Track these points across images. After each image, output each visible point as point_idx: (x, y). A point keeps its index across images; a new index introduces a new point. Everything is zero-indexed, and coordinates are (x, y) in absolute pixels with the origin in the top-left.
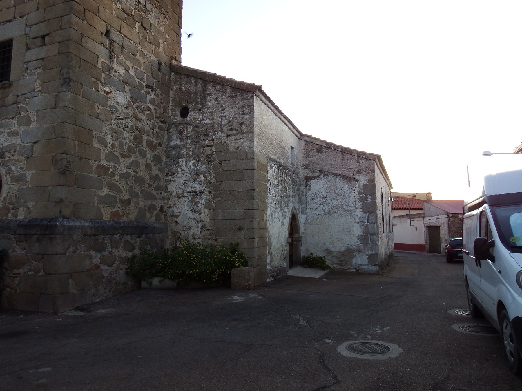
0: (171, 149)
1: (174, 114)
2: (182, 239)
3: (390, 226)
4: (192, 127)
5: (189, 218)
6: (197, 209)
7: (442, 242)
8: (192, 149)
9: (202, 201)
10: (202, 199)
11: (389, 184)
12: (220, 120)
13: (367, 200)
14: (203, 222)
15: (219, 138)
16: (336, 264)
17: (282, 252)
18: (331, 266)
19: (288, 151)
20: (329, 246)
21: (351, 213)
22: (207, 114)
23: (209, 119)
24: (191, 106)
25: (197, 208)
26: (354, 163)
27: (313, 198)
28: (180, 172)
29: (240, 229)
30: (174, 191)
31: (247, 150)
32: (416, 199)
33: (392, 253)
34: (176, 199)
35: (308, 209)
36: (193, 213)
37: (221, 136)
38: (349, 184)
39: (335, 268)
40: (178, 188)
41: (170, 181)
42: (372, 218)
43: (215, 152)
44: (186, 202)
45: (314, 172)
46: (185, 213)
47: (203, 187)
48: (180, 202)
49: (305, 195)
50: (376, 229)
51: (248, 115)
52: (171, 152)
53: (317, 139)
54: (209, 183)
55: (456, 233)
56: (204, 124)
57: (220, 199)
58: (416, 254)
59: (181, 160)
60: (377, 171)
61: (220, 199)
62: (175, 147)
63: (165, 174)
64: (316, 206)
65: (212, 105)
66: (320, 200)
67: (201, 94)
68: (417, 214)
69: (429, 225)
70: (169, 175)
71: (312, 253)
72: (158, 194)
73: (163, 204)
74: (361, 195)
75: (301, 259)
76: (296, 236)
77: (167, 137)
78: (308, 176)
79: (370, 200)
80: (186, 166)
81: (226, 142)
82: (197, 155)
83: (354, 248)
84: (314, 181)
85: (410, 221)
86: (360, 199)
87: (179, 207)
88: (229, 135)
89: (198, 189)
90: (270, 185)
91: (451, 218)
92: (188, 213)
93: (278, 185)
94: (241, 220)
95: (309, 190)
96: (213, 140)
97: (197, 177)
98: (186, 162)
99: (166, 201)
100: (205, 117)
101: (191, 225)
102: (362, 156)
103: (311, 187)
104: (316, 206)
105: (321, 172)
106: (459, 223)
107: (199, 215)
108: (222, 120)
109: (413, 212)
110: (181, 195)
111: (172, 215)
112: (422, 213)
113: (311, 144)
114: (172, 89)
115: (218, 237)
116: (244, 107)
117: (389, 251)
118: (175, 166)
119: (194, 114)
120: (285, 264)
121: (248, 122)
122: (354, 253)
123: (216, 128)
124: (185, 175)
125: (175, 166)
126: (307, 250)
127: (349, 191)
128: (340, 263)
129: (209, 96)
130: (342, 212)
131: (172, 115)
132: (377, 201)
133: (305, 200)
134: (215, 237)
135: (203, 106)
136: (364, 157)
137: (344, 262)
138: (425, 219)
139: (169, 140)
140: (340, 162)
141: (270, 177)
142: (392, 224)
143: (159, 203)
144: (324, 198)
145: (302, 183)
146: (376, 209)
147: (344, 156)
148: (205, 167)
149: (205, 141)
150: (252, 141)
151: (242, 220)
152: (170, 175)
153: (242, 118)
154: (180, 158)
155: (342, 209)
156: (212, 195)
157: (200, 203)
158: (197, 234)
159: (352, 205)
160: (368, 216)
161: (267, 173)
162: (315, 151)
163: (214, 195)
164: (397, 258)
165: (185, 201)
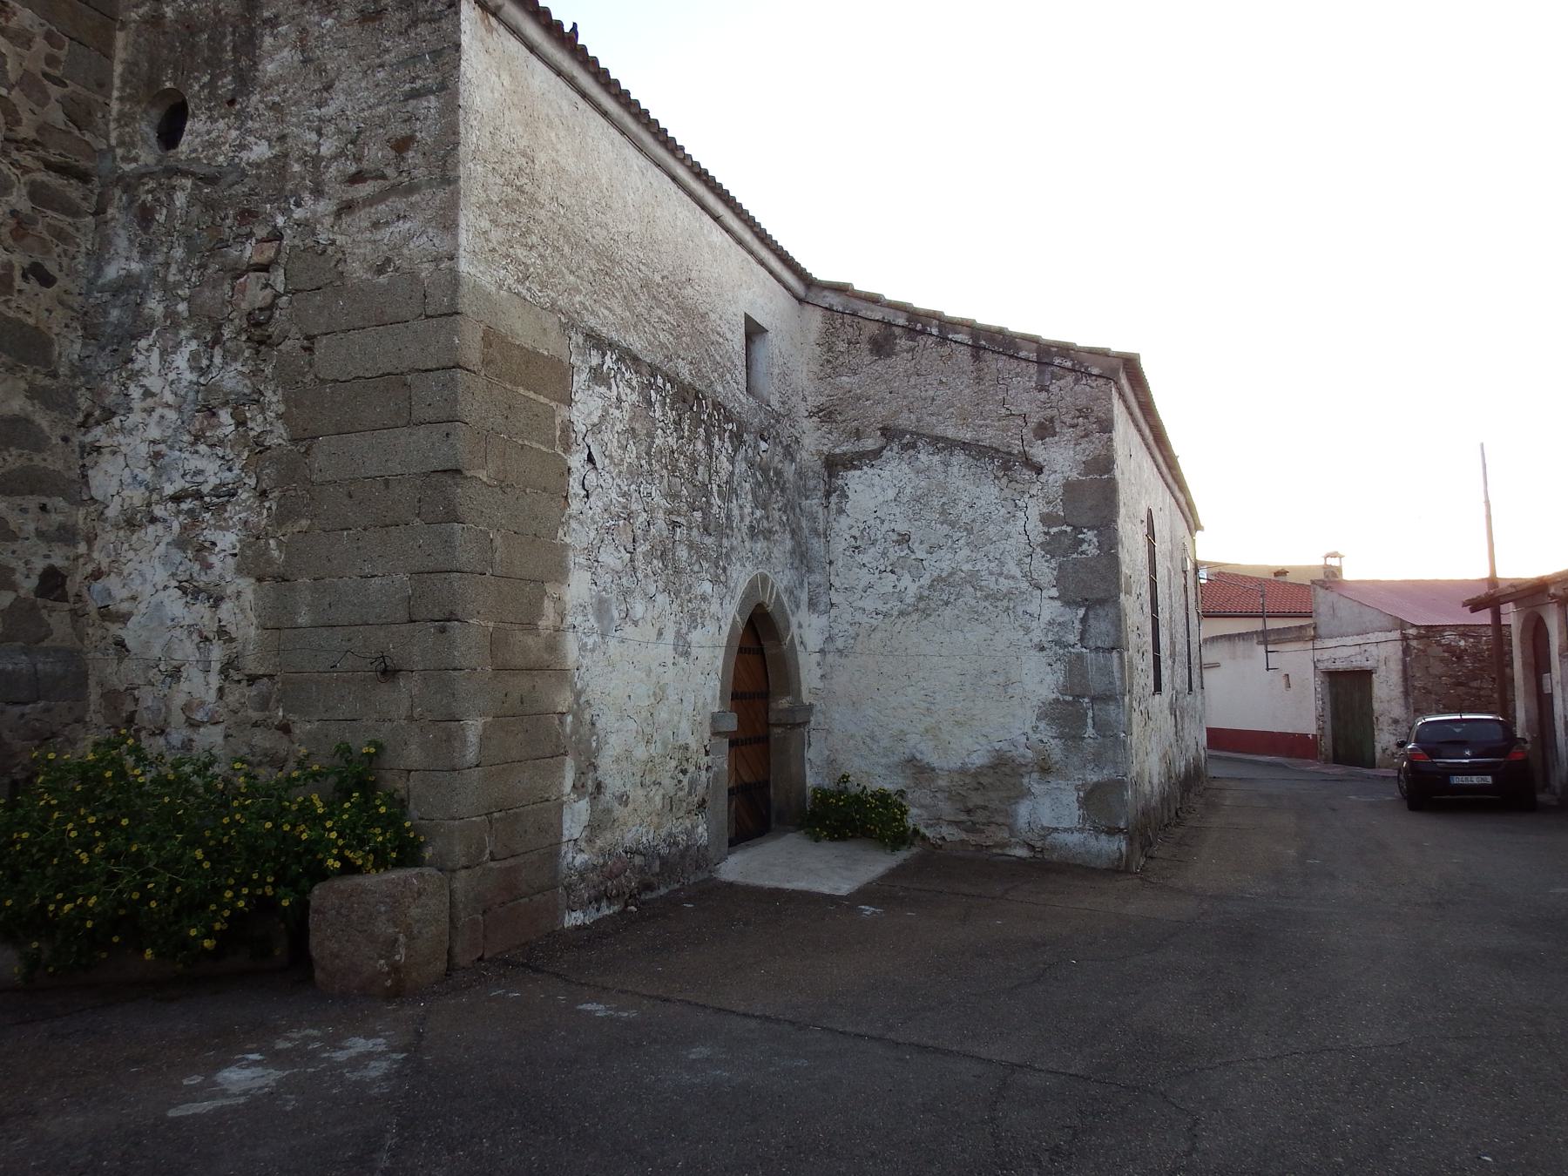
0: (107, 296)
1: (127, 139)
2: (145, 728)
3: (1190, 668)
4: (188, 183)
5: (169, 623)
6: (203, 579)
7: (1380, 727)
8: (187, 290)
9: (227, 540)
10: (227, 529)
11: (1186, 510)
12: (314, 137)
13: (1080, 549)
14: (232, 640)
15: (306, 226)
16: (950, 823)
17: (681, 776)
18: (928, 833)
19: (729, 335)
20: (922, 746)
21: (1011, 606)
22: (259, 116)
23: (269, 140)
24: (197, 88)
25: (203, 573)
26: (1027, 390)
27: (854, 543)
28: (137, 405)
29: (388, 673)
30: (113, 496)
31: (426, 270)
32: (1285, 583)
33: (1197, 767)
34: (121, 533)
35: (836, 589)
36: (190, 596)
37: (314, 212)
38: (1005, 480)
39: (943, 838)
40: (130, 480)
41: (98, 449)
42: (1100, 627)
43: (286, 293)
44: (162, 548)
45: (858, 434)
46: (154, 600)
47: (230, 469)
48: (135, 550)
49: (825, 534)
50: (1117, 675)
51: (432, 97)
52: (106, 313)
53: (874, 300)
54: (259, 448)
55: (1433, 696)
56: (248, 164)
57: (305, 523)
58: (1286, 767)
59: (143, 344)
60: (1126, 438)
61: (305, 523)
62: (127, 286)
63: (80, 418)
64: (865, 577)
65: (280, 72)
66: (884, 554)
67: (237, 27)
68: (1289, 628)
69: (1333, 667)
70: (92, 421)
71: (845, 778)
72: (24, 511)
73: (58, 561)
74: (1054, 530)
75: (809, 801)
76: (784, 703)
77: (93, 245)
78: (834, 455)
79: (1092, 551)
80: (163, 372)
81: (333, 242)
82: (209, 317)
83: (1024, 756)
84: (858, 473)
85: (1267, 652)
86: (1052, 547)
87: (130, 574)
88: (347, 208)
89: (213, 481)
90: (590, 459)
91: (1414, 643)
92: (167, 602)
93: (646, 467)
94: (394, 628)
95: (841, 511)
96: (276, 236)
97: (206, 423)
98: (161, 355)
99: (82, 548)
100: (250, 132)
101: (178, 656)
102: (1057, 361)
103: (847, 497)
104: (865, 577)
105: (888, 433)
106: (1442, 660)
107: (211, 607)
108: (320, 134)
109: (1273, 624)
110: (139, 516)
111: (106, 614)
112: (1309, 626)
113: (848, 319)
114: (124, 26)
115: (292, 717)
116: (415, 58)
117: (1183, 763)
118: (115, 377)
119: (208, 123)
120: (700, 829)
121: (435, 130)
122: (1022, 775)
123: (295, 178)
124: (156, 415)
125: (115, 377)
126: (831, 762)
127: (1003, 511)
128: (963, 817)
129: (268, 31)
130: (973, 602)
131: (121, 143)
132: (1124, 556)
133: (822, 553)
134: (281, 714)
135: (245, 82)
136: (1069, 364)
137: (980, 817)
138: (1318, 644)
139: (98, 258)
140: (967, 391)
141: (588, 422)
142: (1198, 661)
143: (35, 554)
144: (899, 542)
145: (811, 483)
146: (1118, 587)
147: (982, 365)
148: (240, 368)
149: (243, 243)
150: (449, 225)
151: (403, 627)
152: (98, 423)
153: (405, 116)
154: (136, 337)
155: (975, 589)
156: (270, 508)
157: (217, 549)
158: (202, 704)
159: (1016, 571)
160: (1084, 620)
161: (569, 402)
162: (865, 346)
163: (279, 506)
164: (1216, 784)
165: (158, 544)
